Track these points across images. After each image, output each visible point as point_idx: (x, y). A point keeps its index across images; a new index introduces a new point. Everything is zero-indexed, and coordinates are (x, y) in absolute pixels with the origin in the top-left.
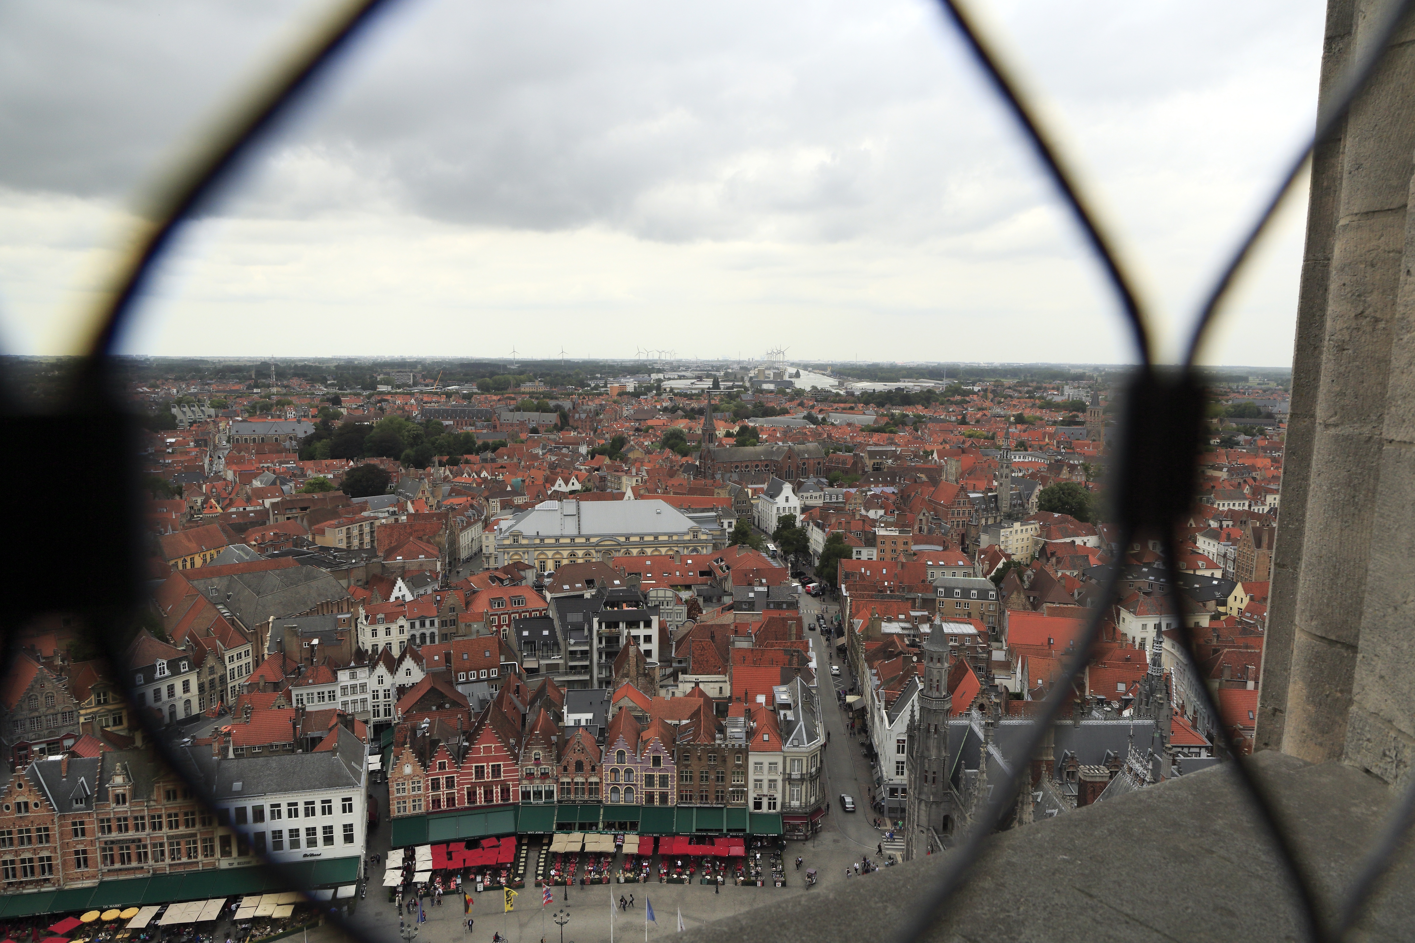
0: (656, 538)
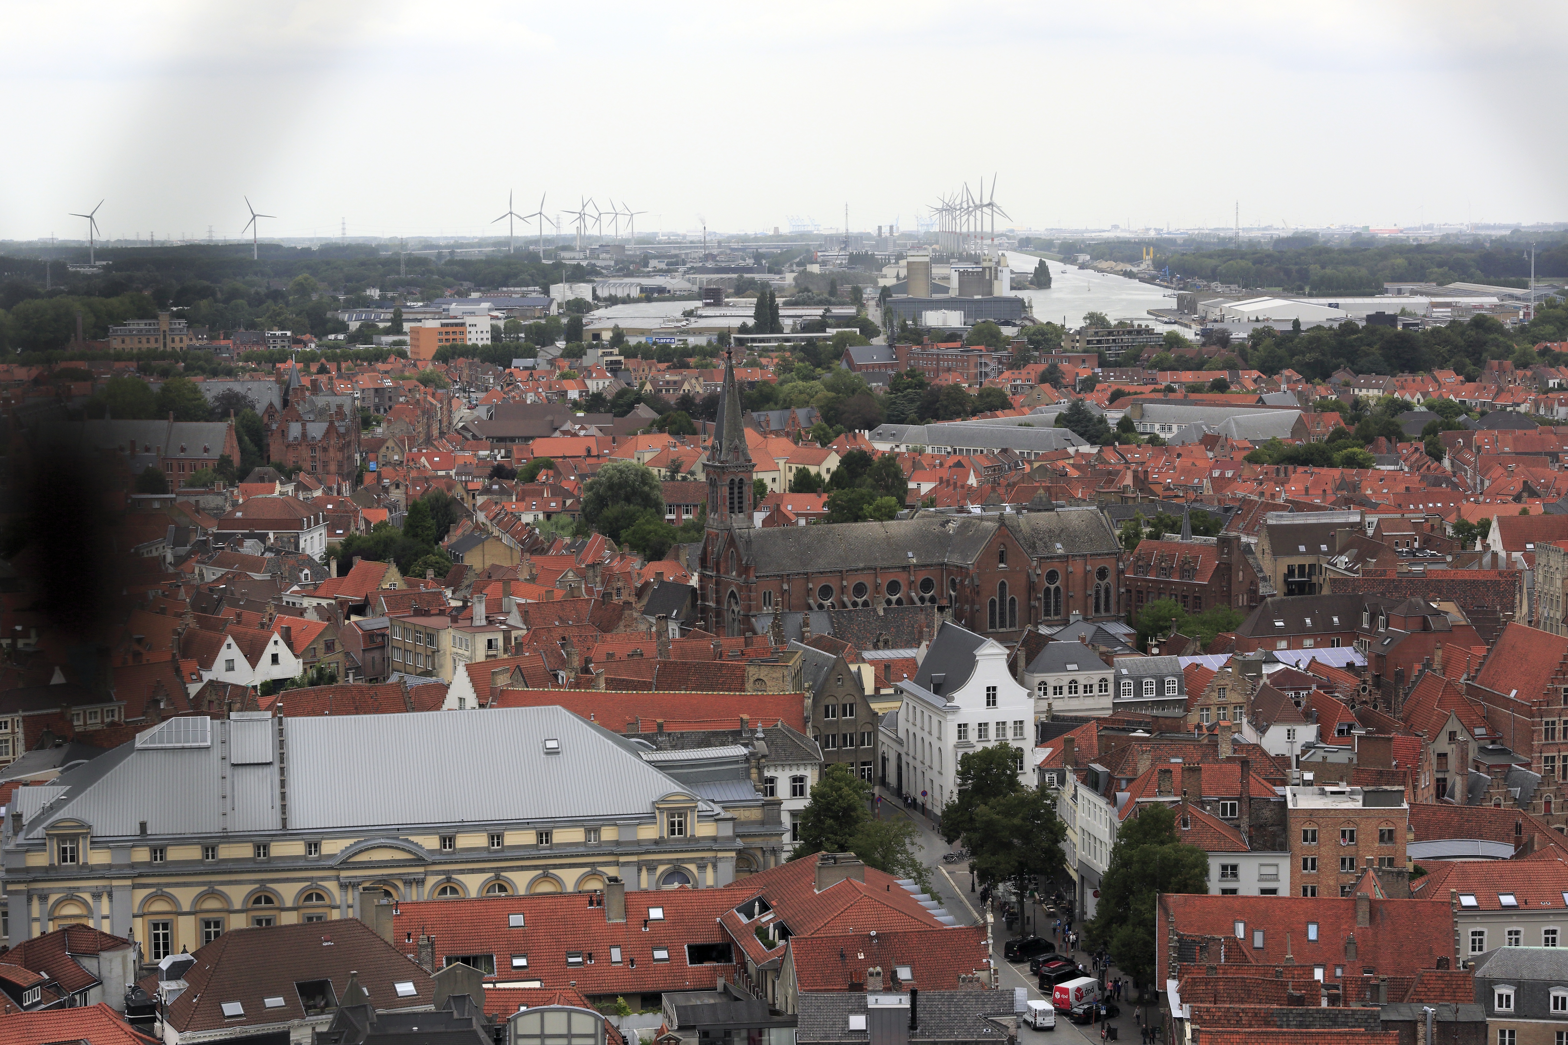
0: (544, 836)
